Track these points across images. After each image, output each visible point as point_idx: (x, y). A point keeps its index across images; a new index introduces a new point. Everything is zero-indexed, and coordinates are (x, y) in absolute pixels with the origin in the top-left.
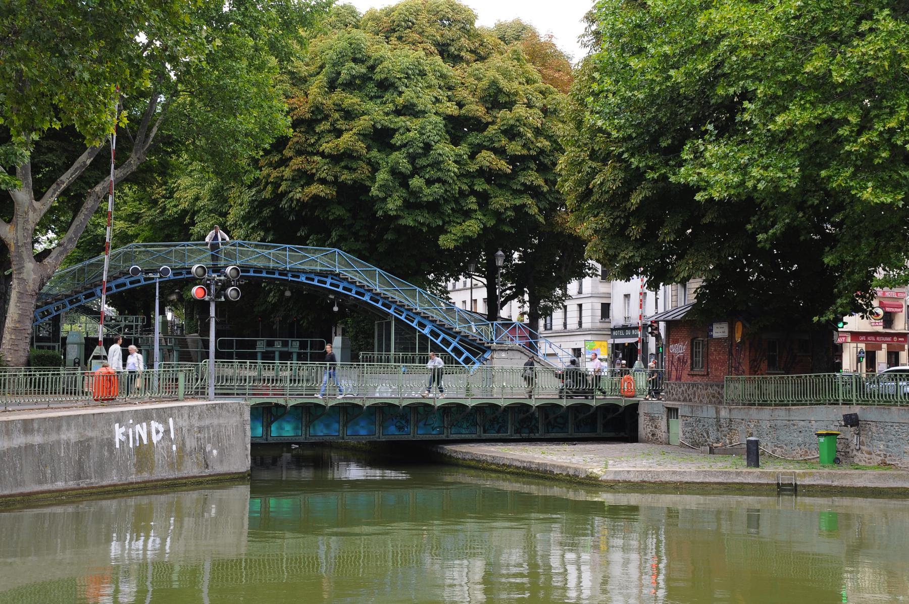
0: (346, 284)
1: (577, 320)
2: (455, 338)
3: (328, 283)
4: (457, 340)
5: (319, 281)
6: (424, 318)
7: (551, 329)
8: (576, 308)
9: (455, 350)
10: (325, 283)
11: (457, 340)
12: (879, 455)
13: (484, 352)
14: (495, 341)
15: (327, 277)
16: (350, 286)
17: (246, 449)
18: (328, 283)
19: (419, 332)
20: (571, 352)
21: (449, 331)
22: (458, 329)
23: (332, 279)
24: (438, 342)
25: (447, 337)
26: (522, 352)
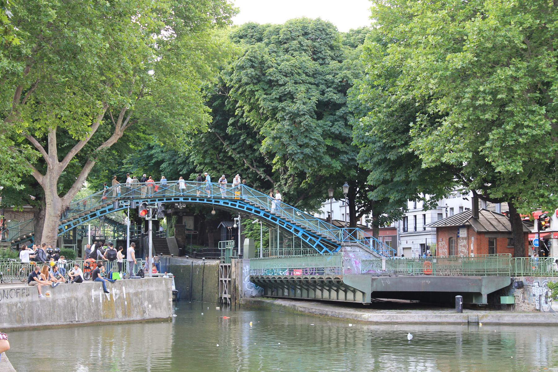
0: (248, 206)
1: (413, 226)
2: (318, 238)
3: (237, 206)
4: (319, 240)
5: (232, 204)
6: (298, 226)
7: (407, 231)
8: (413, 218)
9: (318, 246)
10: (235, 205)
11: (319, 240)
13: (337, 247)
14: (343, 240)
15: (236, 202)
16: (251, 207)
17: (169, 304)
18: (237, 206)
19: (295, 235)
21: (313, 235)
22: (319, 233)
23: (240, 203)
24: (307, 241)
25: (313, 239)
26: (360, 247)
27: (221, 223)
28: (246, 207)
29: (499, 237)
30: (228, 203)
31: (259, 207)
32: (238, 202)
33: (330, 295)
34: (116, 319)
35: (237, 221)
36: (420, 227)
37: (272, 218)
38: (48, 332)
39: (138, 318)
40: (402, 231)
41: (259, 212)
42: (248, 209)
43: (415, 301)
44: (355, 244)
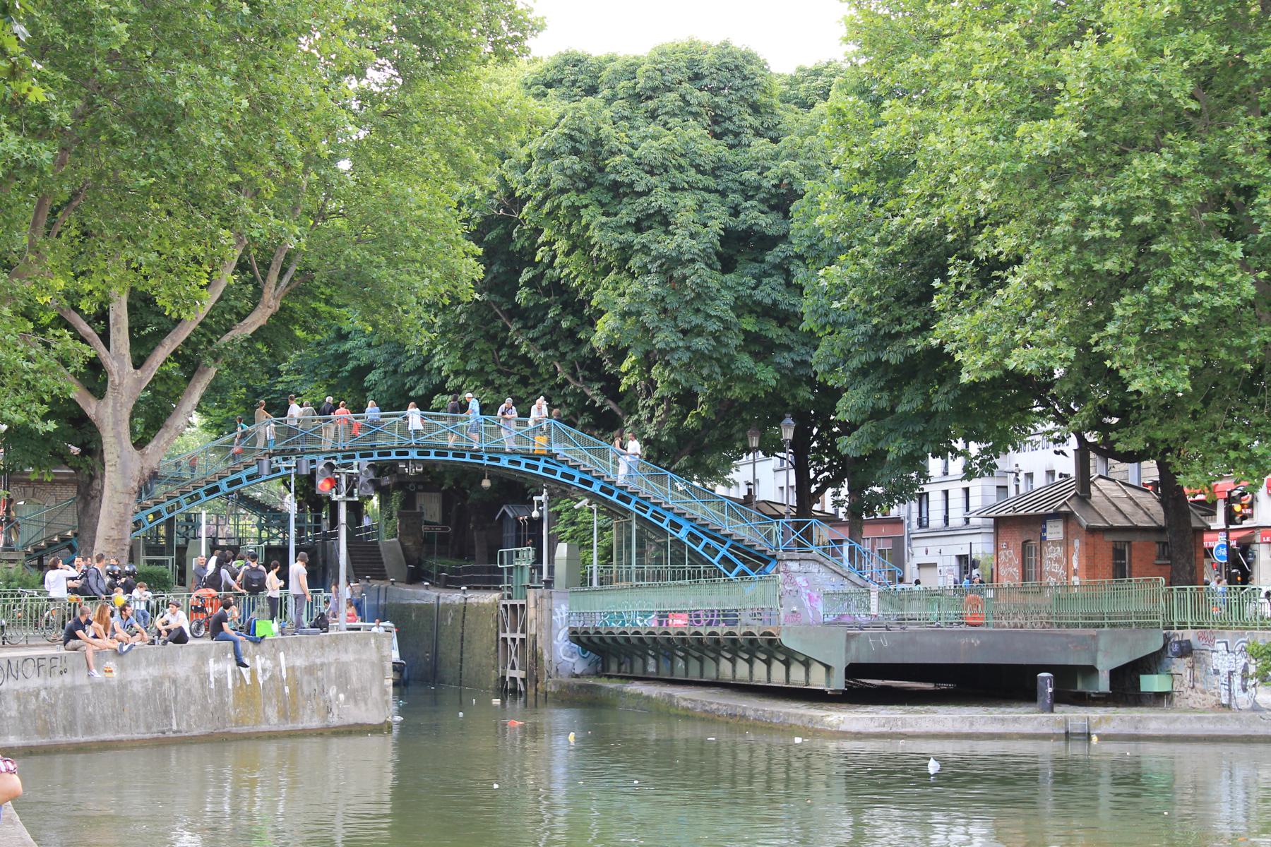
0: (565, 469)
1: (941, 514)
2: (724, 543)
3: (540, 469)
4: (727, 546)
5: (527, 465)
6: (680, 515)
7: (927, 526)
8: (941, 496)
9: (725, 559)
10: (536, 468)
11: (727, 546)
12: (1213, 694)
13: (767, 562)
14: (781, 547)
15: (538, 460)
16: (571, 472)
17: (386, 693)
18: (540, 469)
19: (672, 535)
20: (954, 561)
22: (728, 532)
23: (546, 462)
24: (699, 549)
25: (713, 543)
26: (821, 563)
27: (504, 508)
28: (559, 472)
29: (1138, 540)
30: (519, 463)
31: (590, 472)
32: (543, 459)
33: (751, 672)
34: (264, 727)
35: (540, 503)
36: (956, 518)
37: (620, 497)
38: (108, 756)
39: (315, 723)
40: (915, 525)
41: (589, 484)
42: (564, 475)
43: (944, 686)
44: (809, 556)
